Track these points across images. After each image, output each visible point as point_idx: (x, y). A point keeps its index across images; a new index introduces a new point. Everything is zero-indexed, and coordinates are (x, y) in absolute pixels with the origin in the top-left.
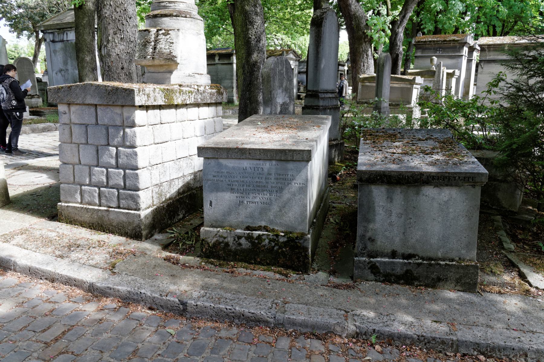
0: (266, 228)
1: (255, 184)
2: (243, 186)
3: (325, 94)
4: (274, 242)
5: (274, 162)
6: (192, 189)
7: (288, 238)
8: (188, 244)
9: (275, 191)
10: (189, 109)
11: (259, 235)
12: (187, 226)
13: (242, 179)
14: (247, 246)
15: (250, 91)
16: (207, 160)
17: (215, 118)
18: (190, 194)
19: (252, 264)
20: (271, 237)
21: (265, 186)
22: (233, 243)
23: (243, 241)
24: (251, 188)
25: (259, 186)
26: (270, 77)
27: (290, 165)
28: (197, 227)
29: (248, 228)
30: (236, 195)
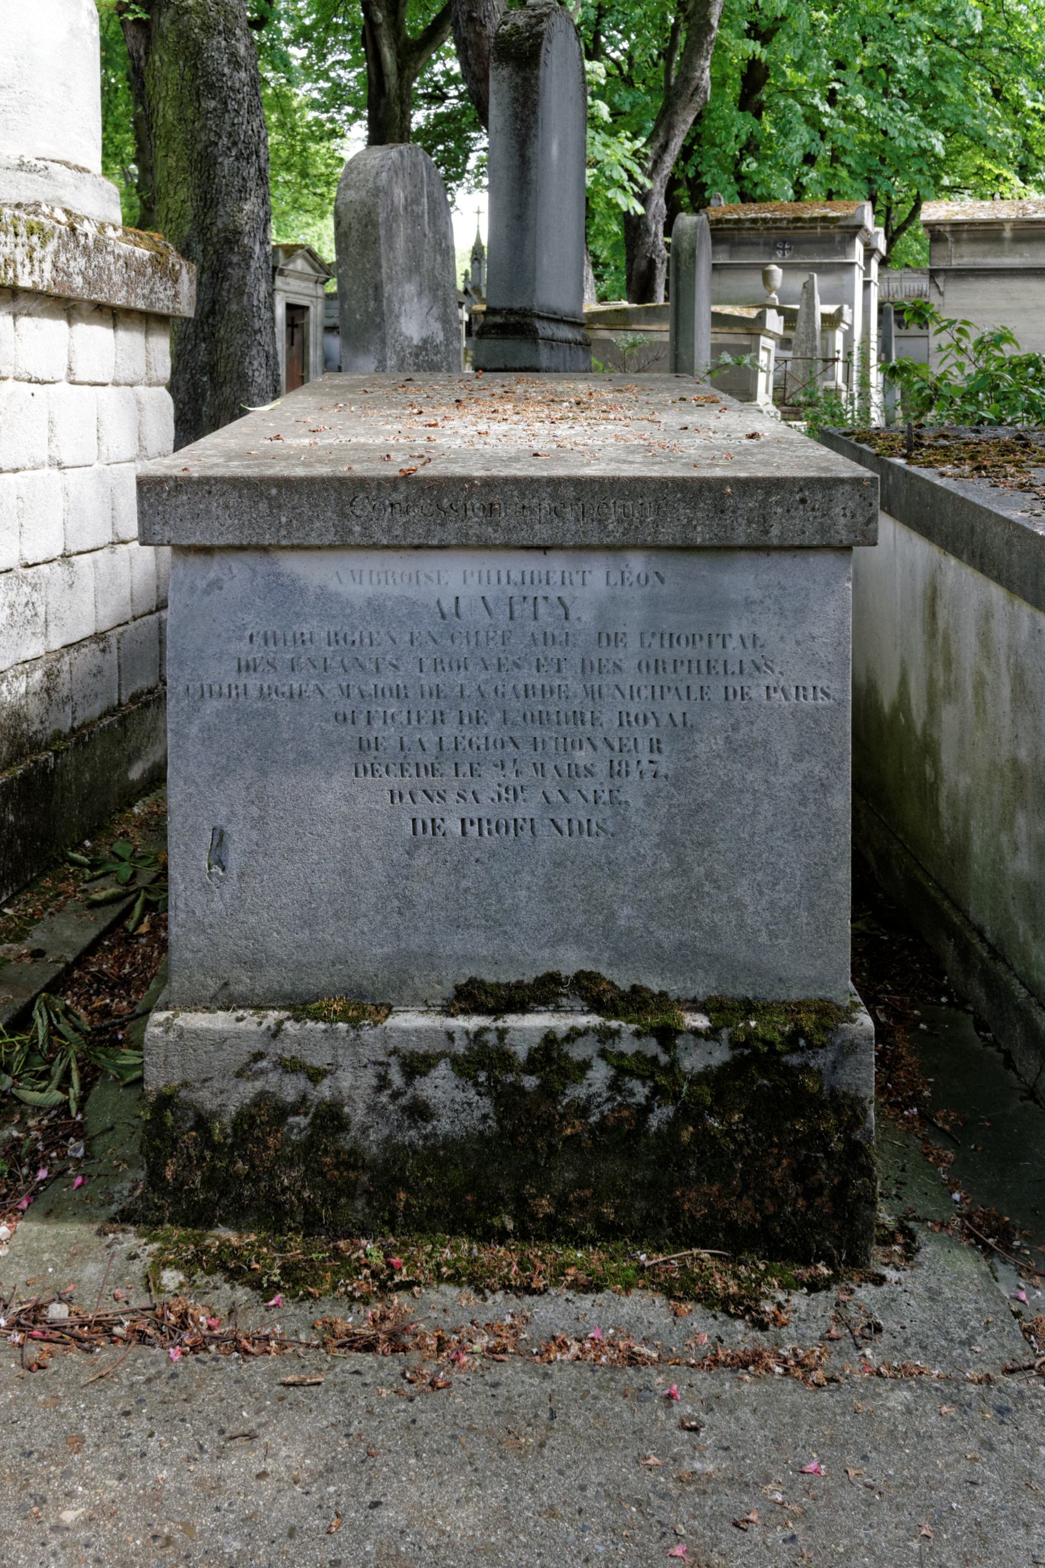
0: (590, 991)
1: (516, 706)
2: (437, 719)
3: (553, 326)
4: (643, 1079)
5: (637, 563)
6: (36, 746)
7: (734, 1044)
8: (38, 1109)
9: (644, 745)
10: (24, 321)
11: (550, 1039)
12: (11, 971)
13: (429, 680)
14: (471, 1120)
15: (212, 339)
16: (196, 561)
17: (140, 389)
18: (25, 778)
19: (502, 1236)
20: (627, 1046)
21: (578, 717)
22: (371, 1108)
23: (439, 1086)
24: (491, 729)
25: (542, 718)
26: (375, 225)
27: (742, 578)
28: (69, 968)
29: (470, 997)
30: (394, 781)
